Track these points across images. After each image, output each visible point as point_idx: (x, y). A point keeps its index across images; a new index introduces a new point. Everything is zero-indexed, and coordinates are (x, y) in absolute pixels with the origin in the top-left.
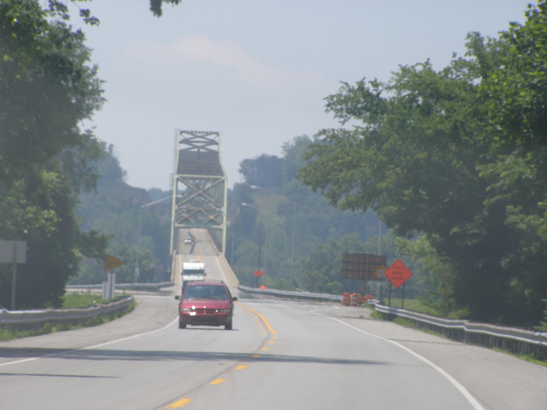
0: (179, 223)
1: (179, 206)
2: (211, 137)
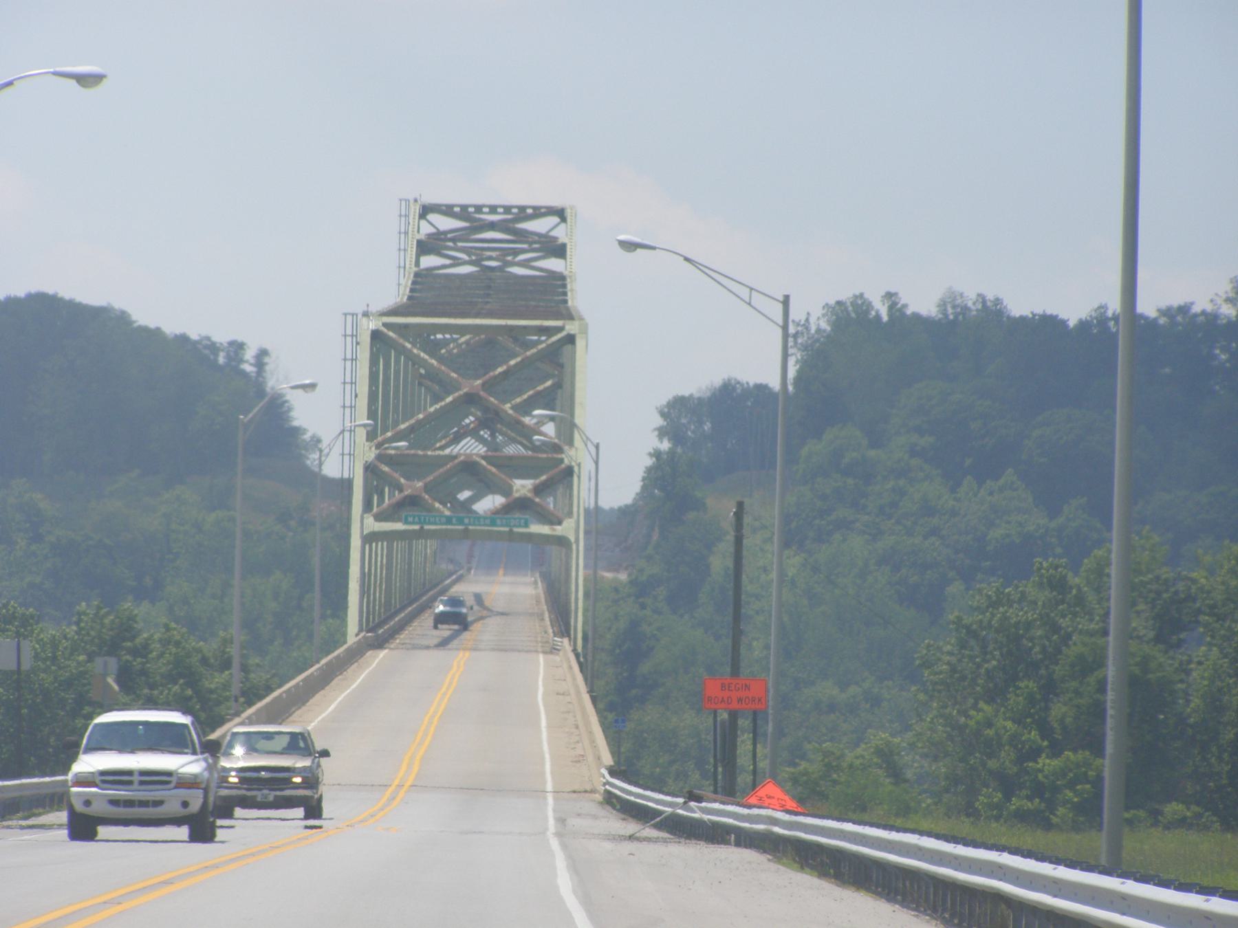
0: (379, 518)
1: (378, 446)
2: (539, 226)
